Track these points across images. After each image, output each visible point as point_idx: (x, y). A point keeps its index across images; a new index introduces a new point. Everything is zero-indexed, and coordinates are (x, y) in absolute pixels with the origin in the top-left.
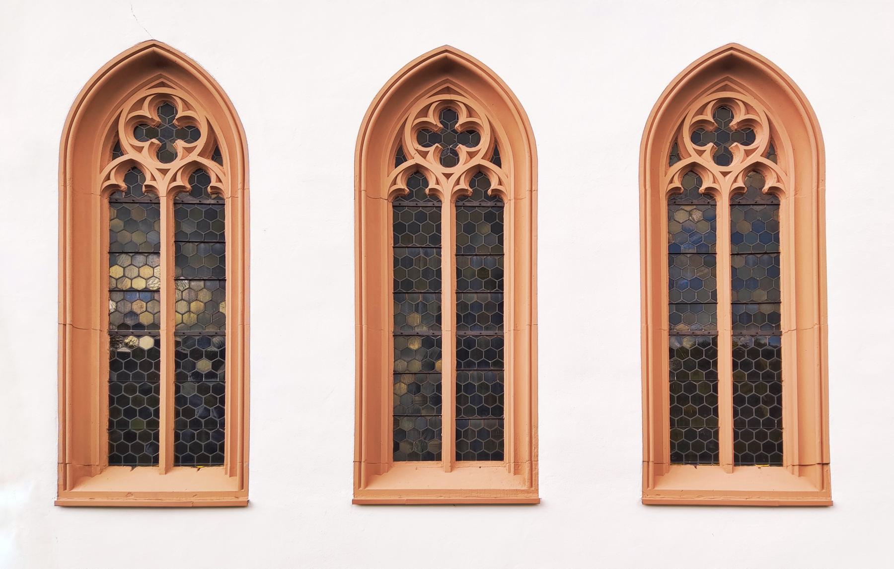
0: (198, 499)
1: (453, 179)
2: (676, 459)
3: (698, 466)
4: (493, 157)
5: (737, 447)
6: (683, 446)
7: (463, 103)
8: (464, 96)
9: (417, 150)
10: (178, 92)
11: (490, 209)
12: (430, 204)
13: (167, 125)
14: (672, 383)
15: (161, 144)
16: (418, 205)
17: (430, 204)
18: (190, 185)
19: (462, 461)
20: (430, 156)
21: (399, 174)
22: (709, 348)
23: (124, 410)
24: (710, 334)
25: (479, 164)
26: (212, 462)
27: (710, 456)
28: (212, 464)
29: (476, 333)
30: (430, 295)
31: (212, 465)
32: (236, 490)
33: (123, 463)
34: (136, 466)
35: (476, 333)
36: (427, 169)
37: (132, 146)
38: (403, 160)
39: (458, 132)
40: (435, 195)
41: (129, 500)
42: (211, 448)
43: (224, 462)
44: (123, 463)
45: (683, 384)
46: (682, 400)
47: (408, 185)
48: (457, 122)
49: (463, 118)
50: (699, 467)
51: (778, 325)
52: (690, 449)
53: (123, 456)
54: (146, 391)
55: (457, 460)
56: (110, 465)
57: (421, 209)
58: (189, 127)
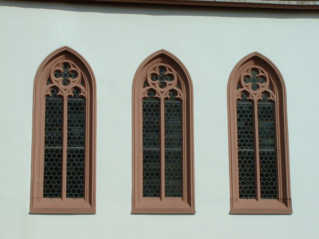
1: (67, 91)
6: (48, 191)
11: (176, 104)
16: (151, 102)
29: (171, 149)
30: (155, 135)
33: (244, 198)
34: (52, 198)
35: (171, 149)
50: (54, 199)
54: (71, 169)
57: (269, 105)
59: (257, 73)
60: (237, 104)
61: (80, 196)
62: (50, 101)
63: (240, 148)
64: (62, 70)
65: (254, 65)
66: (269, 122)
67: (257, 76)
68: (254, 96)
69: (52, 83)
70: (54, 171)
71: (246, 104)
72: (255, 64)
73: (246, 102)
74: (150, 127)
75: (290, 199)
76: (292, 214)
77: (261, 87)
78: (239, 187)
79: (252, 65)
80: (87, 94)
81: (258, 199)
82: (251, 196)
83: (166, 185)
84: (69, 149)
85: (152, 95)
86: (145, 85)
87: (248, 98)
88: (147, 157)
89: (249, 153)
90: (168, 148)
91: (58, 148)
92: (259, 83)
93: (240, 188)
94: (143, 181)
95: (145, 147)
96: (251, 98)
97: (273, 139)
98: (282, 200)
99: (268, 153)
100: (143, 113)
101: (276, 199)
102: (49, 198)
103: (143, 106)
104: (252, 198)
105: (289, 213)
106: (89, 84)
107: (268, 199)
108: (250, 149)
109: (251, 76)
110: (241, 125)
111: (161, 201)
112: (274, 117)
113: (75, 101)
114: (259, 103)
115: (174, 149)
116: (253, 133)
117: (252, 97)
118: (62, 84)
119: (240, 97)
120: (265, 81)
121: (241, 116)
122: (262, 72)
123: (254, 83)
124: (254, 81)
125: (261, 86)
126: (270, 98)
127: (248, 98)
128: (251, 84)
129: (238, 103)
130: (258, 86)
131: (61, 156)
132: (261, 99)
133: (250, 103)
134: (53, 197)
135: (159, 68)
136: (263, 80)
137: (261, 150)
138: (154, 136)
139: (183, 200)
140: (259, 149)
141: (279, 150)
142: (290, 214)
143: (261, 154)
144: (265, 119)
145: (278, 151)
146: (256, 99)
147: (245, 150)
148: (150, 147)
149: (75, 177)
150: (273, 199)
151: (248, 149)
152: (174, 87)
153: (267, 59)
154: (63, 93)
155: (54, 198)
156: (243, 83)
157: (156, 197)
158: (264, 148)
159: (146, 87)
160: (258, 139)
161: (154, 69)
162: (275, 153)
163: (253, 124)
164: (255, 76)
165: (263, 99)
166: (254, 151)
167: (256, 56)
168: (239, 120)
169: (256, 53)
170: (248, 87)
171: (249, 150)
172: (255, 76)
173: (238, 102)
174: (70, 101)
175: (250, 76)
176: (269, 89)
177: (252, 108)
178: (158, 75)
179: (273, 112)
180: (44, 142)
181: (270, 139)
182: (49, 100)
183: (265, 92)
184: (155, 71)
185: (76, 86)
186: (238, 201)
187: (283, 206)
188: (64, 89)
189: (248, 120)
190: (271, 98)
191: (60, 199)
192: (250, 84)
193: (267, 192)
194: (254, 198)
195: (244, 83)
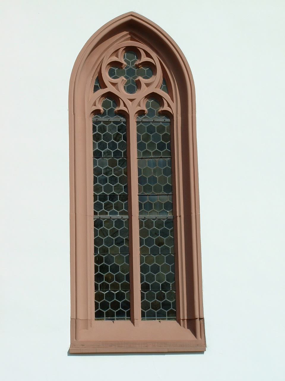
1: (136, 102)
4: (162, 85)
5: (144, 306)
6: (104, 306)
14: (96, 255)
18: (146, 108)
26: (157, 317)
28: (168, 318)
34: (114, 319)
44: (105, 318)
45: (104, 256)
46: (104, 269)
50: (116, 322)
52: (109, 308)
59: (137, 58)
60: (94, 122)
61: (168, 316)
63: (98, 212)
64: (123, 61)
65: (131, 40)
66: (161, 158)
67: (138, 62)
68: (129, 103)
69: (105, 86)
71: (113, 121)
72: (132, 39)
73: (112, 117)
75: (202, 319)
76: (205, 352)
77: (143, 86)
78: (96, 294)
79: (127, 40)
80: (175, 107)
81: (135, 321)
82: (120, 315)
84: (144, 219)
86: (98, 85)
87: (118, 107)
89: (119, 223)
92: (140, 78)
93: (98, 297)
95: (98, 212)
96: (122, 107)
97: (170, 194)
98: (186, 321)
99: (159, 223)
100: (94, 143)
101: (176, 319)
103: (94, 128)
104: (124, 319)
105: (200, 349)
106: (179, 90)
107: (157, 319)
108: (121, 214)
109: (125, 63)
110: (102, 164)
111: (134, 325)
112: (171, 147)
114: (140, 119)
116: (126, 180)
117: (125, 105)
118: (125, 91)
119: (100, 107)
120: (153, 74)
121: (102, 146)
122: (148, 55)
123: (131, 78)
124: (130, 73)
125: (145, 84)
126: (163, 107)
127: (117, 109)
128: (125, 79)
129: (96, 118)
130: (138, 84)
131: (129, 232)
132: (144, 111)
133: (122, 118)
134: (115, 317)
135: (125, 52)
136: (150, 71)
137: (143, 216)
139: (181, 325)
140: (140, 213)
141: (180, 216)
142: (202, 352)
143: (144, 224)
145: (178, 218)
146: (132, 110)
147: (108, 216)
150: (169, 319)
151: (116, 213)
152: (157, 89)
153: (154, 26)
154: (127, 107)
156: (106, 78)
159: (99, 89)
160: (138, 194)
161: (116, 53)
162: (172, 223)
163: (126, 162)
164: (133, 63)
165: (148, 110)
166: (128, 219)
167: (131, 21)
168: (97, 154)
169: (132, 15)
170: (116, 85)
171: (119, 216)
172: (133, 63)
173: (97, 117)
174: (142, 122)
175: (121, 64)
176: (161, 90)
177: (124, 129)
178: (123, 66)
179: (170, 138)
181: (163, 192)
182: (100, 122)
183: (154, 97)
184: (117, 56)
186: (91, 326)
187: (187, 334)
188: (128, 98)
189: (117, 154)
190: (166, 108)
191: (129, 322)
192: (121, 80)
193: (155, 306)
194: (127, 319)
195: (109, 77)
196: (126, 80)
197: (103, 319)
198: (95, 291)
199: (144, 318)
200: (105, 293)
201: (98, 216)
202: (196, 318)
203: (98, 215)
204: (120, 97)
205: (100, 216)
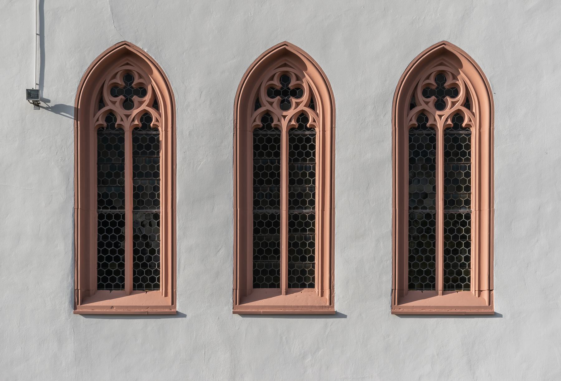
0: (150, 310)
2: (411, 287)
3: (423, 291)
5: (446, 280)
7: (137, 72)
8: (450, 67)
9: (267, 101)
10: (135, 69)
12: (274, 133)
13: (129, 87)
15: (437, 99)
17: (274, 133)
19: (260, 288)
20: (275, 105)
21: (257, 116)
22: (431, 219)
23: (106, 257)
24: (431, 212)
25: (302, 110)
27: (275, 284)
31: (154, 290)
32: (170, 304)
36: (272, 112)
37: (268, 102)
38: (259, 106)
39: (446, 88)
40: (121, 129)
41: (112, 311)
42: (153, 280)
43: (160, 288)
47: (417, 121)
48: (133, 82)
49: (137, 81)
51: (123, 200)
53: (105, 284)
55: (253, 288)
56: (98, 290)
57: (113, 135)
58: (141, 88)
62: (269, 136)
70: (113, 247)
74: (265, 175)
83: (291, 269)
85: (269, 122)
88: (261, 224)
90: (449, 208)
91: (119, 211)
94: (253, 263)
102: (106, 290)
113: (144, 135)
115: (264, 211)
138: (271, 190)
144: (456, 158)
148: (266, 208)
149: (146, 257)
155: (114, 290)
157: (275, 287)
158: (453, 207)
180: (97, 203)
182: (307, 135)
185: (144, 109)
196: (437, 99)
197: (120, 290)
198: (409, 269)
199: (446, 289)
200: (416, 270)
201: (256, 211)
202: (481, 290)
203: (412, 210)
204: (432, 113)
205: (258, 211)
